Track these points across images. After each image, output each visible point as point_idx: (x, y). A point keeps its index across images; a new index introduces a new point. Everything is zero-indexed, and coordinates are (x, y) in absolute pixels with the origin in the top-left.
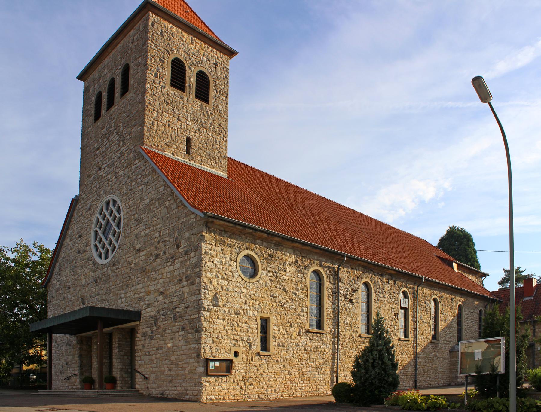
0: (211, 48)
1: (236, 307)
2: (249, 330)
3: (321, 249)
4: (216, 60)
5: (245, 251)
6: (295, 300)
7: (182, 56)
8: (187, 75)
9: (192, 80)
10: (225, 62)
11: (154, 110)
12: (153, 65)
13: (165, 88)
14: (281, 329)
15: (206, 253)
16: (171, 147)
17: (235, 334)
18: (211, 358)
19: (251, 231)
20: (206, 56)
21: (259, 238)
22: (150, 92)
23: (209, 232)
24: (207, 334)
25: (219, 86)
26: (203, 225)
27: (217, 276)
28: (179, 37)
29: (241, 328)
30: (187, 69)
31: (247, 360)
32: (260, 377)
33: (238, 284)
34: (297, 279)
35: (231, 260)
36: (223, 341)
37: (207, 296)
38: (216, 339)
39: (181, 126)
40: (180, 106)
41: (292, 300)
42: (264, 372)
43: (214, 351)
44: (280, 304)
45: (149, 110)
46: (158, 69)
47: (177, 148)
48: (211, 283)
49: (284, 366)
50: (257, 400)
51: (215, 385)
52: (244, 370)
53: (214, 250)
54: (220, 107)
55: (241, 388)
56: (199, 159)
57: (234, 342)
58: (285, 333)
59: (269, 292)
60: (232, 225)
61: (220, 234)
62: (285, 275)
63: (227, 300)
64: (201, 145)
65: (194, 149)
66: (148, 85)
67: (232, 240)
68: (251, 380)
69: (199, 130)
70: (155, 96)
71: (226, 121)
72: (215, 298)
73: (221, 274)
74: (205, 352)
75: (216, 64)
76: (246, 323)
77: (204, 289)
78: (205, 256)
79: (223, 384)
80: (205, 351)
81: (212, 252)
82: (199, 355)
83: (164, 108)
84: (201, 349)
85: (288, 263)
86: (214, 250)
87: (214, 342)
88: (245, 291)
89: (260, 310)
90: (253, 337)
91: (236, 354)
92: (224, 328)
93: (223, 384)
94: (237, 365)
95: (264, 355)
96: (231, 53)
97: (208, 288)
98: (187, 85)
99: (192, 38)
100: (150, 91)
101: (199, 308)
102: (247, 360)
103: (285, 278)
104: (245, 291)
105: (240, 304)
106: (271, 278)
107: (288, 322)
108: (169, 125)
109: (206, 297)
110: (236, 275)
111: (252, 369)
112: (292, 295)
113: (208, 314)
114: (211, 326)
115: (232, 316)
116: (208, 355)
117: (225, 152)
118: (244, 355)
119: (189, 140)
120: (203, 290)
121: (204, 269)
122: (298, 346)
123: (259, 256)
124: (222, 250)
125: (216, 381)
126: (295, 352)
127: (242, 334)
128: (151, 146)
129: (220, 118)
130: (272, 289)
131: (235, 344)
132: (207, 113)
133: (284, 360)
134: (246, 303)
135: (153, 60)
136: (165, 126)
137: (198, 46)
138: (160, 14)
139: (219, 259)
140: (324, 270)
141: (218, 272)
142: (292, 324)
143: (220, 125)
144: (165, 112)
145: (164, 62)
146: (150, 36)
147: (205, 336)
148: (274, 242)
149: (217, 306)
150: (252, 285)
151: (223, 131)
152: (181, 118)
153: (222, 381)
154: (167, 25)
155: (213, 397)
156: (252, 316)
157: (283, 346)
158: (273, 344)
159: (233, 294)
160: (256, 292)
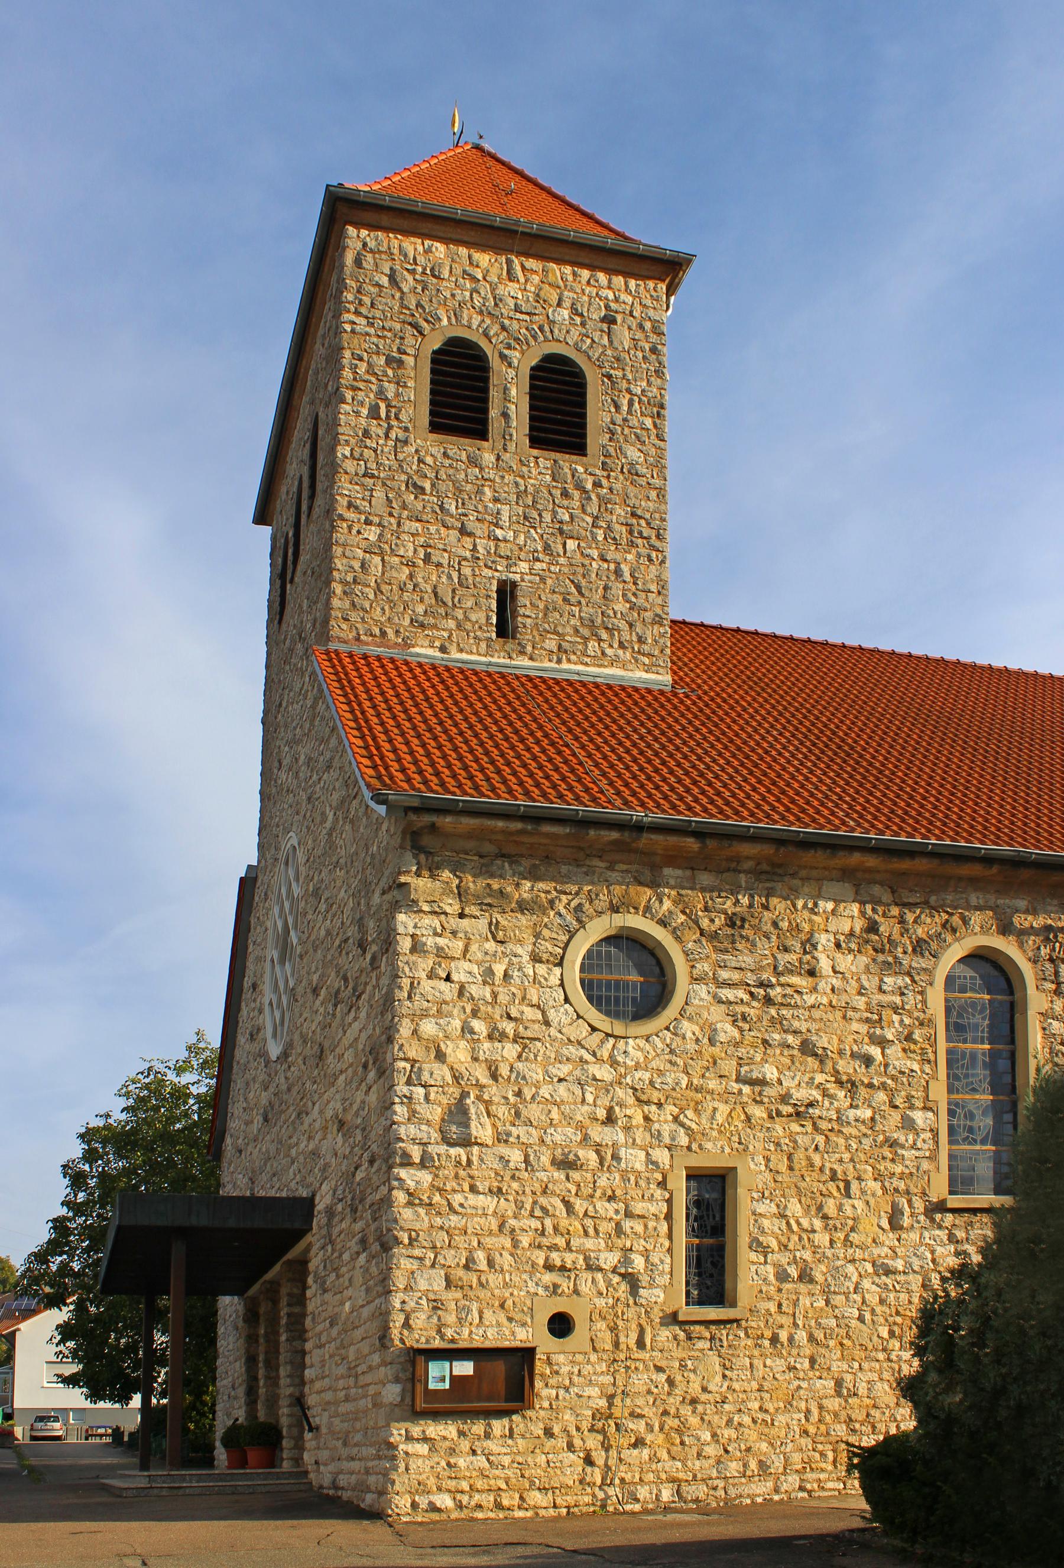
0: (585, 274)
1: (558, 1138)
2: (627, 1225)
3: (988, 860)
4: (607, 307)
5: (606, 918)
6: (870, 1086)
7: (472, 327)
8: (494, 380)
9: (513, 392)
10: (648, 302)
11: (368, 522)
12: (361, 385)
13: (406, 442)
14: (795, 1208)
15: (417, 948)
16: (435, 627)
17: (554, 1247)
18: (437, 1343)
19: (615, 835)
20: (567, 304)
21: (673, 859)
22: (351, 469)
23: (433, 871)
24: (417, 1252)
25: (625, 385)
26: (402, 847)
27: (467, 1029)
28: (458, 271)
29: (589, 1222)
30: (495, 362)
31: (616, 1345)
32: (686, 1410)
33: (572, 1051)
34: (878, 997)
35: (536, 959)
36: (494, 1280)
37: (423, 1109)
38: (461, 1273)
39: (474, 549)
40: (469, 487)
41: (851, 1086)
42: (704, 1389)
43: (451, 1318)
44: (787, 1109)
45: (350, 528)
46: (381, 394)
47: (459, 626)
48: (440, 1056)
49: (813, 1361)
50: (667, 1510)
51: (452, 1451)
52: (602, 1386)
53: (454, 933)
54: (633, 453)
55: (589, 1461)
56: (551, 644)
57: (548, 1278)
58: (818, 1224)
59: (729, 1066)
60: (519, 825)
61: (485, 870)
62: (814, 990)
63: (518, 1114)
64: (559, 599)
65: (527, 612)
66: (343, 451)
67: (541, 885)
68: (640, 1426)
69: (547, 548)
70: (373, 476)
71: (661, 493)
72: (458, 1113)
73: (489, 1018)
74: (406, 1324)
75: (609, 320)
76: (611, 1198)
77: (409, 1082)
78: (413, 958)
79: (492, 1446)
80: (407, 1319)
81: (441, 941)
82: (384, 1337)
83: (404, 507)
84: (388, 1313)
85: (824, 940)
86: (454, 933)
87: (449, 1283)
88: (605, 1073)
89: (684, 1140)
90: (646, 1254)
91: (561, 1325)
92: (501, 1226)
93: (492, 1446)
94: (565, 1370)
95: (707, 1323)
96: (669, 268)
97: (425, 1077)
98: (494, 413)
99: (509, 262)
100: (350, 466)
101: (387, 1156)
102: (616, 1345)
103: (810, 999)
104: (605, 1073)
105: (580, 1126)
106: (739, 1009)
107: (834, 1177)
108: (427, 559)
109: (413, 1113)
110: (560, 1015)
111: (639, 1381)
112: (847, 1067)
113: (426, 1177)
114: (438, 1221)
115: (542, 1175)
116: (423, 1333)
117: (659, 600)
118: (601, 1325)
119: (506, 593)
120: (402, 1089)
121: (405, 1007)
122: (888, 1272)
123: (674, 931)
124: (494, 928)
125: (461, 1433)
126: (873, 1299)
127: (590, 1244)
128: (358, 639)
129: (632, 491)
130: (742, 1051)
131: (556, 1286)
132: (580, 487)
133: (811, 1338)
134: (610, 1120)
135: (363, 367)
136: (411, 564)
137: (536, 279)
138: (385, 219)
139: (479, 964)
140: (1021, 945)
141: (475, 1013)
142: (855, 1186)
143: (633, 515)
144: (409, 519)
145: (400, 363)
146: (350, 297)
147: (406, 1264)
148: (749, 865)
149: (466, 1142)
150: (639, 1046)
151: (647, 533)
152: (471, 525)
153: (487, 1436)
154: (413, 246)
155: (445, 1501)
156: (639, 1166)
157: (806, 1276)
158: (751, 1274)
159: (545, 1092)
160: (660, 1073)
